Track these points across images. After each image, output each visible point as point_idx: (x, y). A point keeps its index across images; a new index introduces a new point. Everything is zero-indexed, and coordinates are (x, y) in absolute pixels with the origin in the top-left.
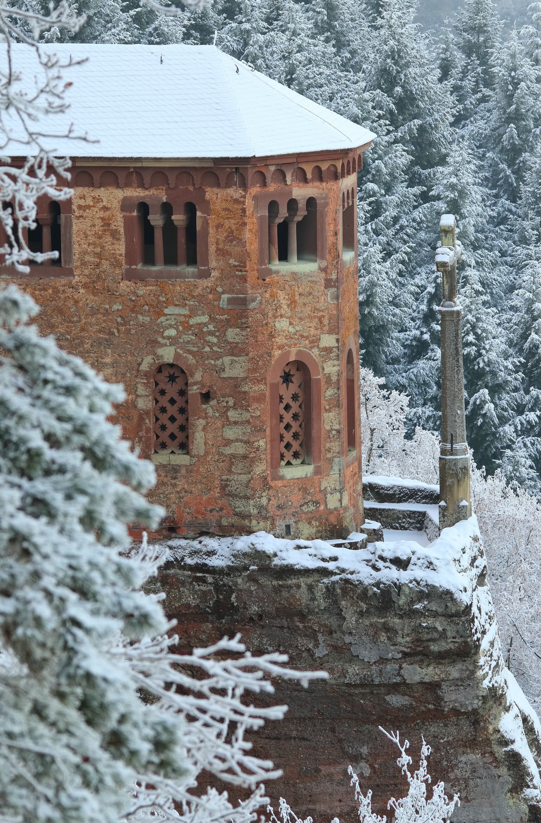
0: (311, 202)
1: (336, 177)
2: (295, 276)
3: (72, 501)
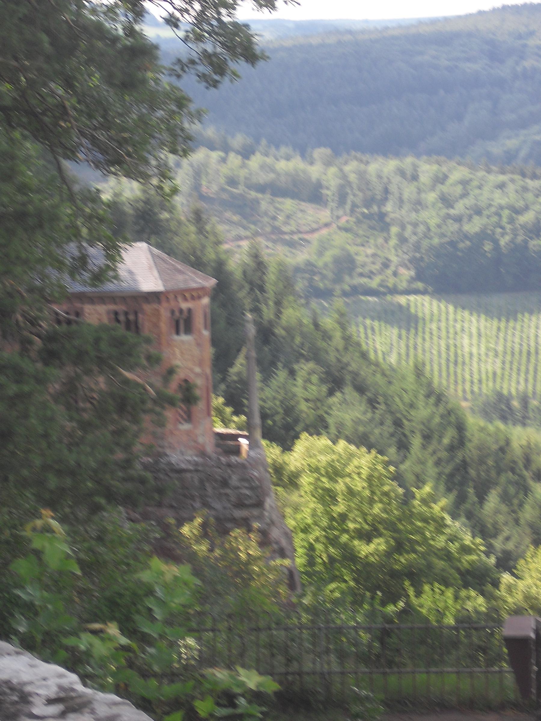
0: (190, 310)
1: (199, 297)
2: (183, 342)
3: (187, 378)
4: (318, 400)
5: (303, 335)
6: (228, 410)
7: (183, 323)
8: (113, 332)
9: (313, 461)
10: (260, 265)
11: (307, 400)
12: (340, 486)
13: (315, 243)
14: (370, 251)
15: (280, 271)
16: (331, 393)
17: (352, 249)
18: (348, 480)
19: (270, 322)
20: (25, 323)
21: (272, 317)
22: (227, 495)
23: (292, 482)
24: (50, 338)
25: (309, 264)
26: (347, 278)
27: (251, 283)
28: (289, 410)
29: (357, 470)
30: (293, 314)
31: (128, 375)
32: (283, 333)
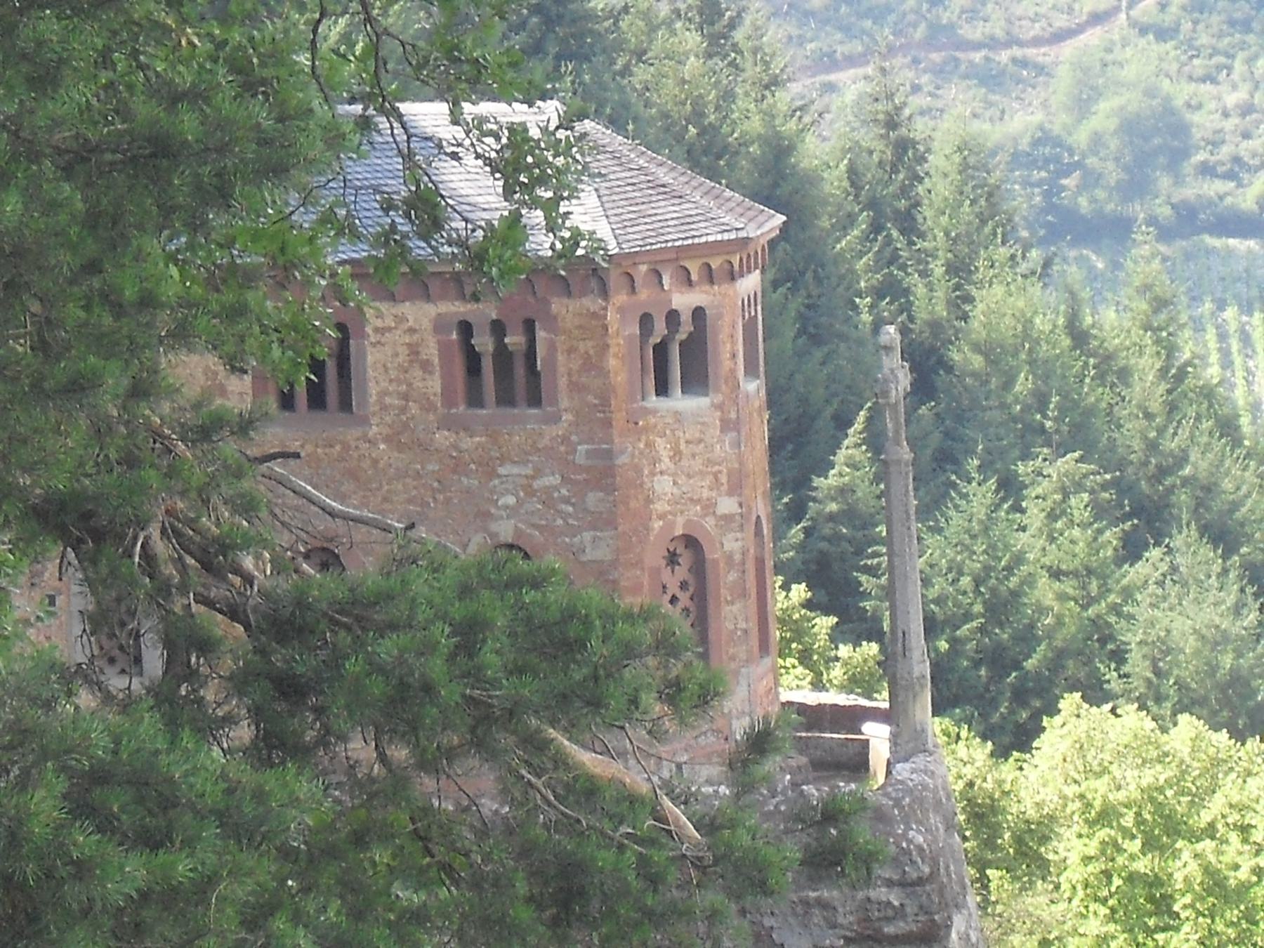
0: (698, 313)
4: (1090, 572)
5: (1043, 370)
6: (824, 623)
7: (680, 356)
8: (529, 596)
9: (1099, 789)
10: (905, 154)
11: (1056, 574)
12: (1184, 867)
13: (1064, 78)
14: (1232, 99)
15: (964, 167)
16: (1131, 550)
17: (1182, 93)
18: (1207, 845)
19: (935, 326)
20: (183, 569)
21: (941, 311)
22: (823, 905)
23: (1029, 853)
24: (284, 624)
25: (1044, 138)
26: (1164, 182)
27: (872, 204)
28: (1001, 607)
29: (1233, 818)
30: (1006, 302)
31: (587, 759)
32: (977, 361)
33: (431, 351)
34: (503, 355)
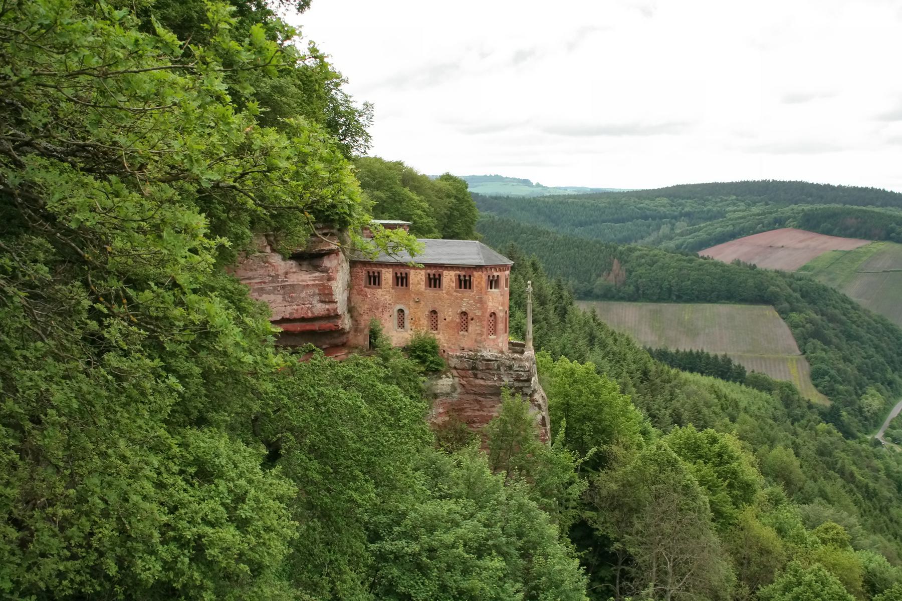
7: (493, 283)
33: (454, 280)
34: (465, 281)
